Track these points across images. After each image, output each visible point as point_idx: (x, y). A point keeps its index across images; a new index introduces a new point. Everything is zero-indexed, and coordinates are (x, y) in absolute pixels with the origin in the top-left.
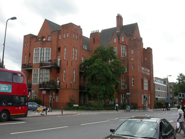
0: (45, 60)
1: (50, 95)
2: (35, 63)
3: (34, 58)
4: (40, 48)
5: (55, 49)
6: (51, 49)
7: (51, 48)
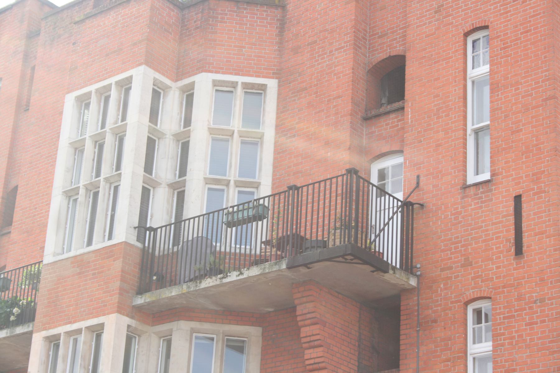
0: (196, 205)
1: (151, 131)
2: (78, 249)
3: (57, 201)
4: (142, 78)
5: (341, 71)
6: (272, 84)
7: (277, 74)
